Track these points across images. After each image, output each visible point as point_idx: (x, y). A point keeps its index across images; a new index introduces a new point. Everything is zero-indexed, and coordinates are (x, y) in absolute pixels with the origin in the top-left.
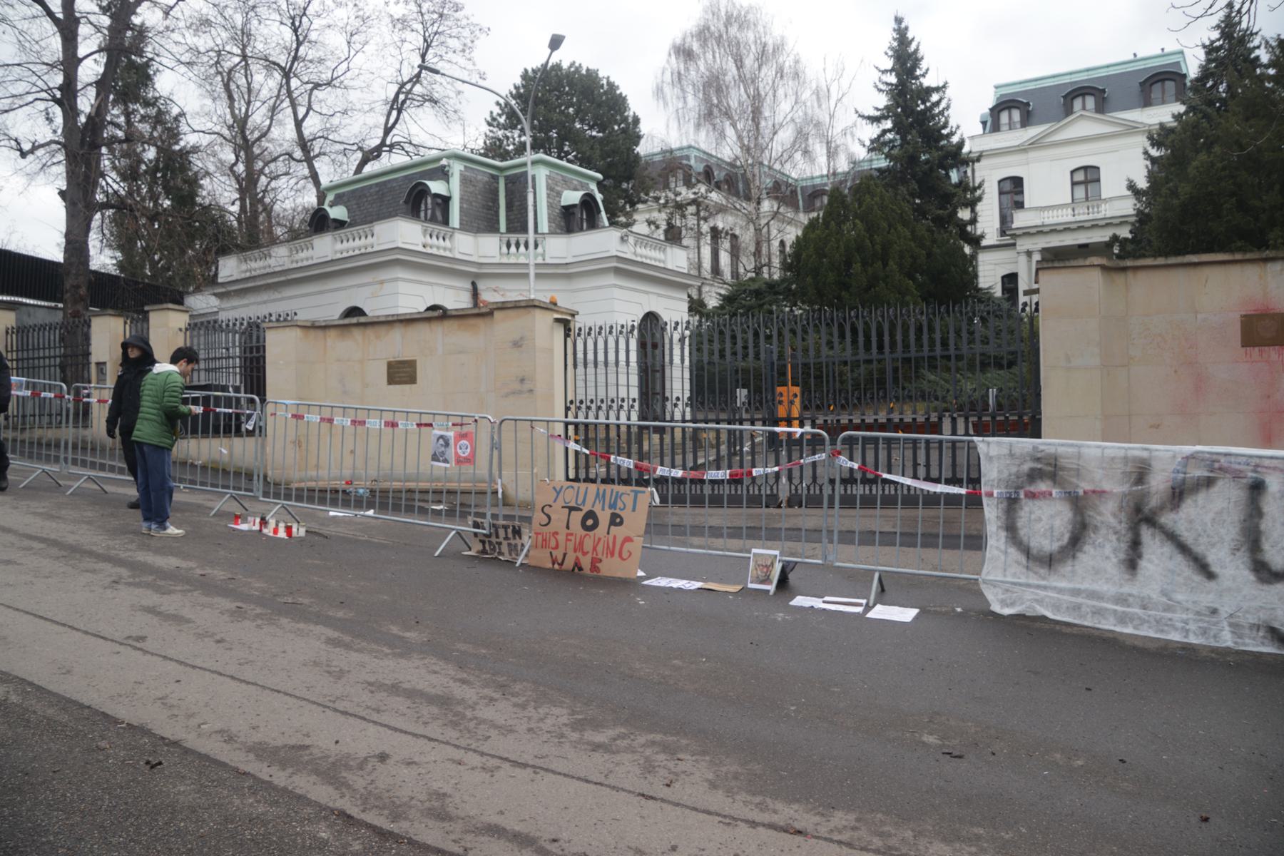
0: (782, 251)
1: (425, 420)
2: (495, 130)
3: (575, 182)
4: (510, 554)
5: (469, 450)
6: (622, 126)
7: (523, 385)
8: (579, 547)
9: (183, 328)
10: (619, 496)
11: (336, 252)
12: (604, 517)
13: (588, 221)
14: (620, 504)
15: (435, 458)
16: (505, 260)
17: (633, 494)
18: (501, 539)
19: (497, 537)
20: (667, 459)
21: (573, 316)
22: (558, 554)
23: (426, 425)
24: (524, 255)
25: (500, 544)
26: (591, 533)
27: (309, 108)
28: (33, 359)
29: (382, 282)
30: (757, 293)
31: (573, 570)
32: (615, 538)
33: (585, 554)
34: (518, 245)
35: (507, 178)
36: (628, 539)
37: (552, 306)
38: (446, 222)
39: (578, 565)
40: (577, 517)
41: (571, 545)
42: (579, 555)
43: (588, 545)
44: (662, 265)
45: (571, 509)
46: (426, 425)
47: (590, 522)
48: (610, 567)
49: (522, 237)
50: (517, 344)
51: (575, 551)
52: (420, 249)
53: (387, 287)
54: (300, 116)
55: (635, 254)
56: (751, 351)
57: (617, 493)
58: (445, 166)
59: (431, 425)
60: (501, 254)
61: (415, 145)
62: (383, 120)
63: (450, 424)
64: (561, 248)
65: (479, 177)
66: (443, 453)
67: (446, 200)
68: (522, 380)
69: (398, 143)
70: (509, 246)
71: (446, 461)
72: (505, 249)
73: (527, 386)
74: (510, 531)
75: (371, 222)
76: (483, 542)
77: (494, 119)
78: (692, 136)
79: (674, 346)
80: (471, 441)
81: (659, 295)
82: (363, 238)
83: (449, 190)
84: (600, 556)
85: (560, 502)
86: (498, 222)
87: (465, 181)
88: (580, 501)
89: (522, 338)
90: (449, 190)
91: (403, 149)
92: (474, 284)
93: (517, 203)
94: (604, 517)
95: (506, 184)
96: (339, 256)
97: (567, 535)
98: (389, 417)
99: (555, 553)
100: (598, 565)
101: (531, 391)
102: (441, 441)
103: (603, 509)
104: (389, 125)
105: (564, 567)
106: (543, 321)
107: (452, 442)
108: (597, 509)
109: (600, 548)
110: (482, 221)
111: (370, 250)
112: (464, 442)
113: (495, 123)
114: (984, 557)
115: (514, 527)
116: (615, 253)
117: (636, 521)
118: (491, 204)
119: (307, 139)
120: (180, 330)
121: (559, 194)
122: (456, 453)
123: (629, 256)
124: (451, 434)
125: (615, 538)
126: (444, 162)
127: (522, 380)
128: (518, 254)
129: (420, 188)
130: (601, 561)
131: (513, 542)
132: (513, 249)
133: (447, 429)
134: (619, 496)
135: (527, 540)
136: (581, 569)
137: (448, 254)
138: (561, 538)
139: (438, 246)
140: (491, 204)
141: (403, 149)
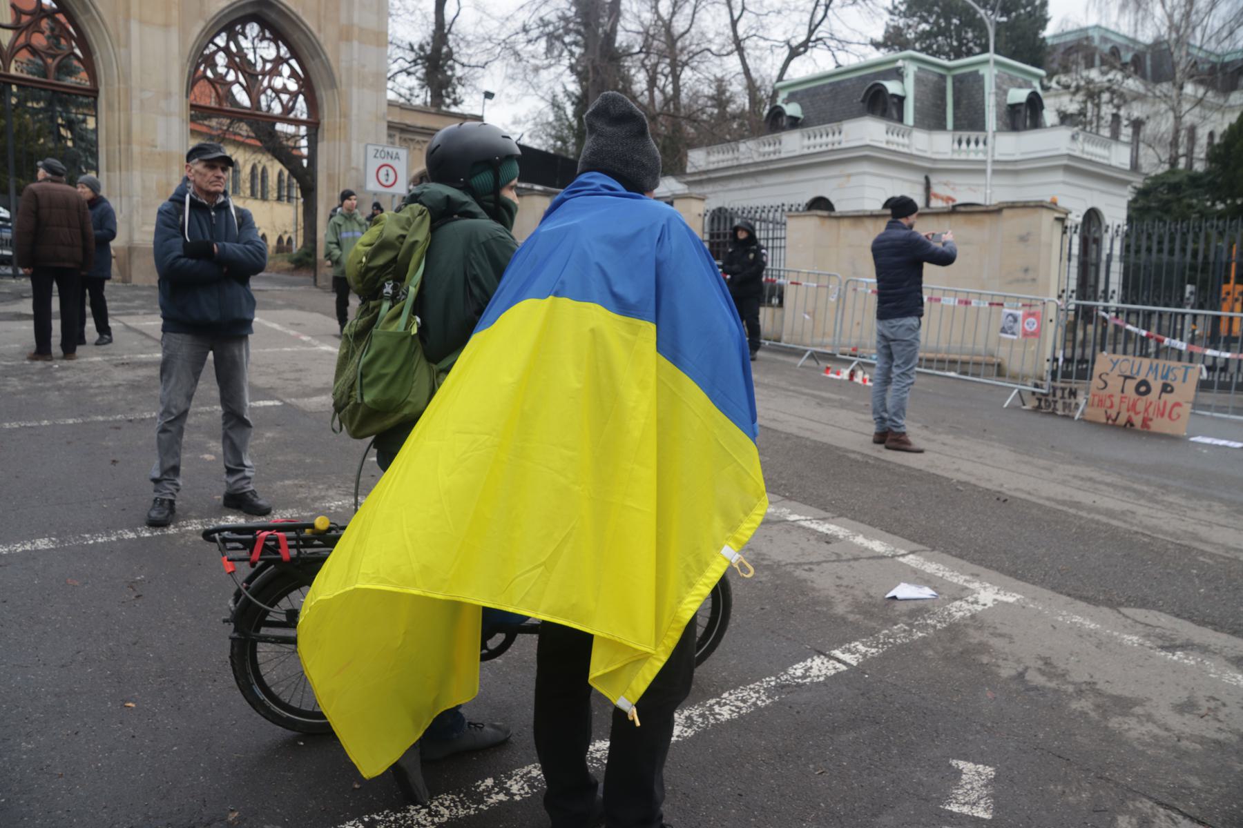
0: (1210, 144)
1: (996, 300)
2: (896, 18)
3: (1020, 80)
4: (1064, 410)
5: (1035, 326)
6: (1029, 9)
7: (1028, 275)
8: (1133, 408)
9: (702, 213)
10: (1170, 369)
11: (803, 147)
12: (1156, 386)
13: (1031, 118)
14: (1171, 376)
15: (1003, 330)
16: (956, 157)
17: (1183, 369)
18: (1058, 397)
19: (1054, 395)
20: (1120, 347)
21: (1067, 214)
22: (1113, 413)
23: (998, 304)
24: (974, 151)
25: (1055, 402)
26: (1144, 398)
27: (744, 9)
28: (773, 239)
29: (849, 176)
30: (1175, 188)
31: (1125, 425)
32: (1165, 403)
33: (1137, 413)
34: (968, 142)
35: (955, 78)
36: (1177, 404)
37: (1052, 206)
38: (901, 119)
39: (1130, 423)
40: (1131, 385)
41: (1124, 406)
42: (1132, 414)
43: (1141, 406)
44: (1105, 161)
45: (1126, 378)
46: (998, 304)
47: (1143, 389)
48: (1158, 425)
49: (981, 135)
50: (1023, 239)
51: (1128, 410)
52: (884, 145)
53: (854, 180)
54: (736, 17)
55: (1083, 151)
56: (1166, 246)
57: (1169, 367)
58: (900, 68)
59: (1002, 305)
60: (953, 151)
61: (840, 41)
62: (807, 18)
63: (1020, 304)
64: (1011, 145)
65: (931, 77)
66: (1011, 328)
67: (901, 100)
68: (1026, 270)
69: (820, 39)
70: (960, 142)
71: (1013, 334)
72: (956, 146)
73: (1030, 275)
74: (1067, 392)
75: (840, 121)
76: (1040, 400)
77: (895, 8)
78: (1114, 18)
79: (275, 187)
80: (1037, 318)
81: (1102, 192)
82: (830, 136)
83: (904, 90)
84: (1151, 416)
85: (1117, 371)
86: (945, 119)
87: (918, 81)
88: (1135, 371)
89: (1028, 234)
90: (904, 90)
91: (825, 44)
92: (927, 179)
93: (965, 102)
94: (1156, 386)
95: (954, 83)
96: (806, 151)
97: (1122, 398)
98: (963, 297)
99: (1109, 411)
100: (1149, 423)
101: (1034, 280)
102: (1010, 318)
103: (1156, 379)
104: (816, 21)
105: (1117, 422)
106: (1047, 218)
107: (1020, 319)
108: (1150, 379)
109: (1151, 410)
110: (932, 119)
111: (837, 146)
112: (1032, 319)
113: (897, 12)
114: (610, 643)
115: (1071, 390)
116: (1065, 151)
117: (1186, 390)
118: (939, 102)
119: (740, 38)
120: (700, 215)
121: (1006, 92)
122: (1024, 328)
123: (1077, 153)
124: (1020, 313)
125: (1165, 403)
126: (900, 63)
127: (1026, 270)
128: (968, 152)
129: (876, 88)
130: (1151, 420)
131: (1068, 401)
132: (964, 145)
133: (1017, 308)
134: (1170, 369)
135: (1081, 400)
136: (1132, 425)
137: (905, 150)
138: (1116, 400)
139: (972, 153)
140: (939, 102)
141: (825, 44)
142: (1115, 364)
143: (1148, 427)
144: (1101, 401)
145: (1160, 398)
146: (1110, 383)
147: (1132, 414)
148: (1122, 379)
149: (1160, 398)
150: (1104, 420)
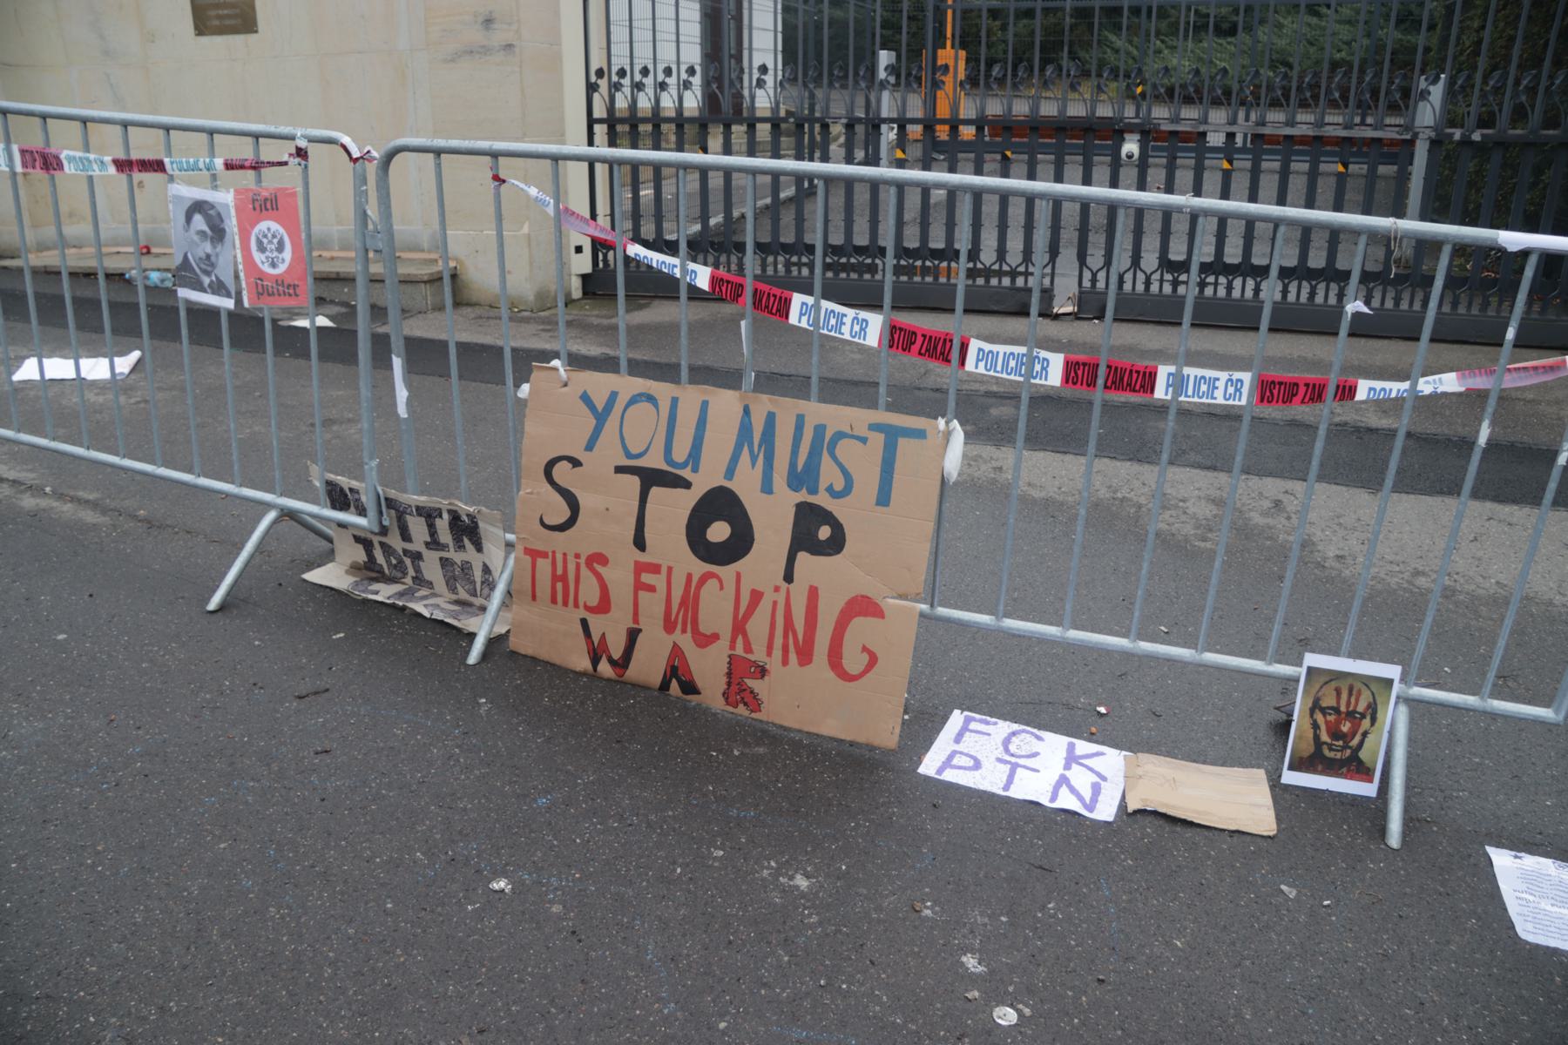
8: (683, 614)
10: (824, 442)
14: (829, 474)
17: (878, 439)
18: (418, 545)
25: (417, 557)
26: (727, 572)
36: (862, 606)
40: (669, 510)
41: (653, 606)
43: (716, 609)
45: (651, 479)
47: (719, 532)
59: (158, 166)
66: (209, 262)
68: (488, 22)
73: (499, 36)
74: (443, 524)
85: (609, 453)
88: (681, 452)
97: (640, 568)
99: (597, 624)
101: (509, 47)
102: (199, 222)
107: (232, 224)
108: (746, 486)
109: (758, 627)
115: (455, 517)
127: (488, 22)
130: (762, 672)
134: (824, 442)
136: (690, 688)
138: (619, 576)
142: (601, 417)
143: (754, 702)
144: (559, 578)
145: (789, 577)
146: (584, 499)
147: (685, 641)
148: (634, 482)
149: (789, 577)
150: (584, 664)
